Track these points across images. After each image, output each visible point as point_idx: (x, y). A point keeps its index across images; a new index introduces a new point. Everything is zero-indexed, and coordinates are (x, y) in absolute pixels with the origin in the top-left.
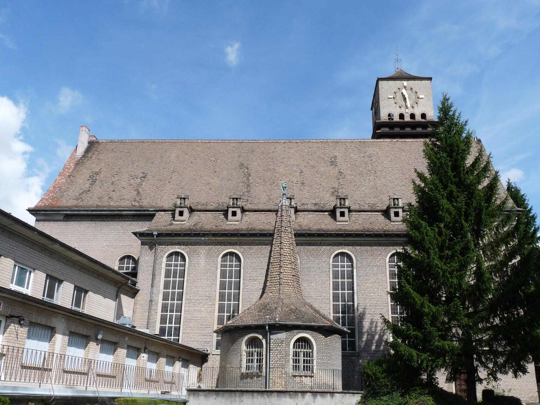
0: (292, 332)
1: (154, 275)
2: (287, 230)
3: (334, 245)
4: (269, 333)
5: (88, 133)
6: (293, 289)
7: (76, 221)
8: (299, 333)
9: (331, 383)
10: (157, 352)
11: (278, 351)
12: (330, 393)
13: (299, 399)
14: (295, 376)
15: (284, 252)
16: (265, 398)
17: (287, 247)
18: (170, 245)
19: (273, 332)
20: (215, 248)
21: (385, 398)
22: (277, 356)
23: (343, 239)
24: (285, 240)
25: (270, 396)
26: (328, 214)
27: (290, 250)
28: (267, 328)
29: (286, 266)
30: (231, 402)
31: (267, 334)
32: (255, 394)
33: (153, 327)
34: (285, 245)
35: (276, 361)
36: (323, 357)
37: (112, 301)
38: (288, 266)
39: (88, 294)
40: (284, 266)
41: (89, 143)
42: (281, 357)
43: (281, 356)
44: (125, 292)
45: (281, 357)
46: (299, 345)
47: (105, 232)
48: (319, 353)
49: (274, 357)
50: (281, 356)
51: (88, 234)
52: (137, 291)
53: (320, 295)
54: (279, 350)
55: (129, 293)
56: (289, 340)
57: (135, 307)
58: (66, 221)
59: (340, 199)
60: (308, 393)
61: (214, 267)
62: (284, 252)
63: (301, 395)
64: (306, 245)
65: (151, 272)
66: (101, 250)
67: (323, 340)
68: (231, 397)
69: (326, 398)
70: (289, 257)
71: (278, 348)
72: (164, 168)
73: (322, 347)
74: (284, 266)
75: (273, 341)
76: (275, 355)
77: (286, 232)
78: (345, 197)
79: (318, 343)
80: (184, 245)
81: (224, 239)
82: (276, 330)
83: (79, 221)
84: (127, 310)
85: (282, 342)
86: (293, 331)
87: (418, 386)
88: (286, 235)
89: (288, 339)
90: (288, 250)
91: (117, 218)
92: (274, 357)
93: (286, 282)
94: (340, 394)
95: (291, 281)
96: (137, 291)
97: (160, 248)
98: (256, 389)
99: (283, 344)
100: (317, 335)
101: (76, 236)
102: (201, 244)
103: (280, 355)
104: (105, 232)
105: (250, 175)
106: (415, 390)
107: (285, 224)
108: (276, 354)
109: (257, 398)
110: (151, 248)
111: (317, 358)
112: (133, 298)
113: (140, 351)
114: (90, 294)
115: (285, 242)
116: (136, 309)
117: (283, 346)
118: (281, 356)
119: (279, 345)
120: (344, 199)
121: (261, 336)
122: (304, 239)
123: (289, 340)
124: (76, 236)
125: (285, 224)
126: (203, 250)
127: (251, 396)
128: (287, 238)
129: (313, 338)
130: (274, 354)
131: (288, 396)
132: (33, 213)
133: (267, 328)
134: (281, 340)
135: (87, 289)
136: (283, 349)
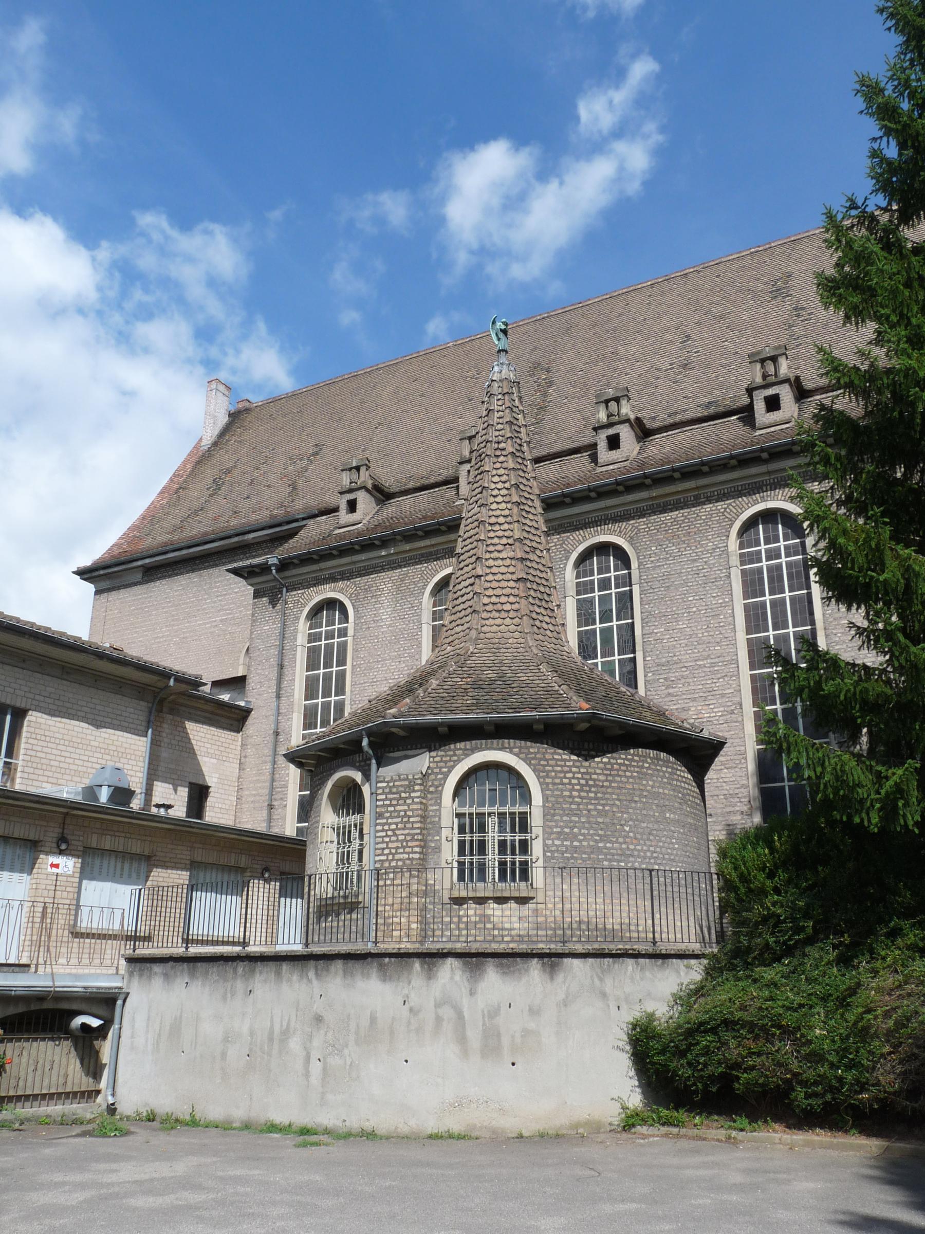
0: (450, 750)
1: (281, 667)
2: (504, 449)
3: (738, 493)
4: (374, 761)
5: (227, 393)
6: (516, 621)
7: (164, 577)
8: (473, 750)
9: (645, 923)
10: (146, 853)
11: (398, 816)
12: (541, 956)
13: (413, 983)
14: (459, 901)
15: (491, 513)
16: (310, 981)
17: (499, 499)
18: (315, 585)
19: (391, 755)
20: (413, 572)
21: (769, 974)
22: (395, 835)
23: (763, 469)
24: (496, 479)
25: (325, 973)
26: (738, 419)
27: (509, 506)
28: (365, 742)
29: (496, 555)
30: (224, 998)
31: (370, 765)
32: (285, 967)
33: (282, 799)
34: (495, 492)
35: (393, 851)
36: (572, 828)
37: (130, 735)
38: (504, 555)
39: (28, 718)
40: (488, 556)
41: (230, 415)
42: (409, 838)
43: (406, 832)
44: (206, 717)
45: (409, 838)
46: (482, 793)
47: (217, 592)
48: (554, 815)
49: (387, 839)
50: (408, 834)
51: (187, 603)
52: (245, 714)
53: (705, 654)
54: (402, 813)
55: (217, 718)
56: (440, 776)
57: (243, 754)
58: (147, 582)
59: (763, 361)
60: (450, 961)
61: (414, 623)
62: (491, 513)
63: (422, 967)
64: (654, 513)
65: (274, 661)
66: (212, 633)
67: (574, 769)
68: (225, 980)
69: (524, 980)
70: (506, 526)
71: (398, 808)
72: (362, 423)
73: (566, 793)
74: (488, 556)
75: (385, 785)
76: (390, 833)
77: (498, 456)
78: (776, 353)
79: (549, 780)
80: (343, 579)
81: (433, 543)
82: (398, 750)
83: (170, 576)
84: (215, 761)
85: (410, 788)
86: (452, 746)
87: (907, 915)
88: (498, 465)
89: (437, 774)
90: (503, 506)
91: (242, 553)
92: (387, 839)
93: (494, 604)
94: (590, 960)
95: (512, 599)
96: (245, 714)
97: (292, 597)
98: (344, 948)
99: (414, 791)
100: (544, 754)
101: (166, 612)
102: (382, 569)
103: (403, 829)
104: (217, 592)
105: (550, 384)
106: (894, 934)
107: (497, 433)
108: (393, 827)
109: (289, 980)
110: (273, 602)
111: (548, 833)
112: (238, 732)
113: (39, 849)
114: (33, 718)
115: (493, 486)
116: (245, 757)
117: (413, 798)
118: (406, 832)
119: (401, 798)
120: (774, 359)
121: (360, 774)
122: (644, 494)
123: (440, 776)
124: (166, 612)
125: (497, 433)
126: (385, 582)
127: (375, 970)
128: (502, 471)
129: (530, 765)
130: (386, 827)
131: (374, 973)
132: (86, 576)
133: (365, 742)
134: (407, 779)
135: (22, 705)
136: (413, 810)
